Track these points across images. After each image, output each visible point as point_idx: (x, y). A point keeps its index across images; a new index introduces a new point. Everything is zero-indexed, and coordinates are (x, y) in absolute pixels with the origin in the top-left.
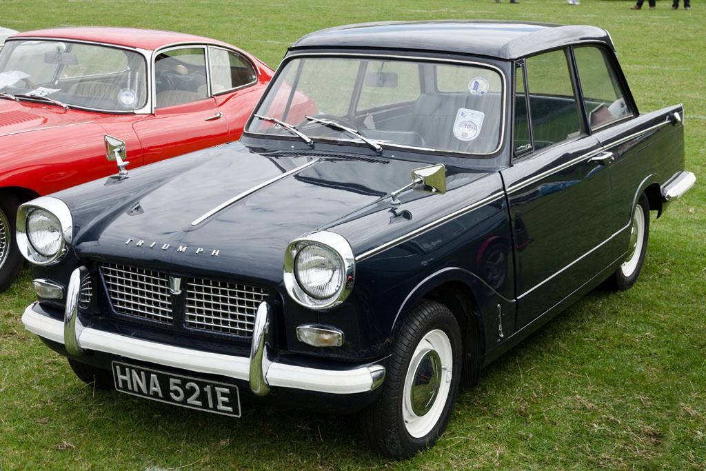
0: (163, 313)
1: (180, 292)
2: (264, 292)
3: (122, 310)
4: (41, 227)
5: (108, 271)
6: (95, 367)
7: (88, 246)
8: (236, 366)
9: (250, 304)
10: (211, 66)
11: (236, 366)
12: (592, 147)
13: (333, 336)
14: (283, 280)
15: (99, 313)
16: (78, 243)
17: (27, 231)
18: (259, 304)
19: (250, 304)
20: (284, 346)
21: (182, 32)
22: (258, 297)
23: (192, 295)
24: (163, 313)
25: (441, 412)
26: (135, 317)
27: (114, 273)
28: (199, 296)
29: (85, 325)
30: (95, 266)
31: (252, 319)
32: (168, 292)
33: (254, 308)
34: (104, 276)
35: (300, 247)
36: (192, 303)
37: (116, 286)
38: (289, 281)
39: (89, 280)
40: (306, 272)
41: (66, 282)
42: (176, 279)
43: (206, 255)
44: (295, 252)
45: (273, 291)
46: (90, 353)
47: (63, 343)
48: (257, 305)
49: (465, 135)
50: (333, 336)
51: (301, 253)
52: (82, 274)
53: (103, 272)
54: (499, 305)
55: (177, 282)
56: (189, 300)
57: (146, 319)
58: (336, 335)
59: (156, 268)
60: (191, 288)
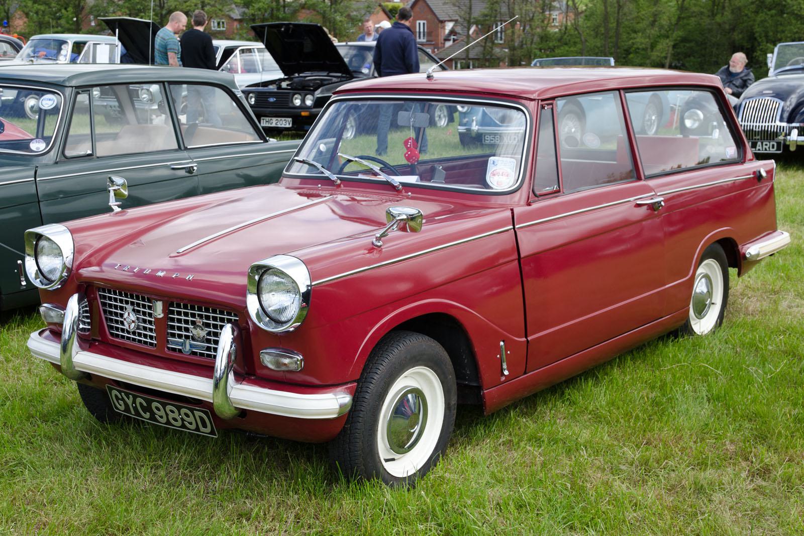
0: (151, 337)
1: (162, 316)
2: (235, 315)
3: (117, 336)
4: (277, 288)
5: (105, 297)
6: (94, 388)
7: (86, 272)
8: (195, 385)
9: (215, 326)
10: (360, 103)
11: (195, 385)
12: (148, 161)
13: (293, 361)
14: (246, 307)
15: (98, 338)
16: (80, 266)
17: (259, 294)
18: (223, 326)
19: (215, 326)
20: (247, 367)
21: (520, 65)
22: (222, 320)
23: (172, 320)
24: (151, 337)
25: (433, 448)
26: (145, 346)
27: (110, 299)
28: (179, 321)
29: (83, 348)
30: (88, 290)
31: (216, 342)
32: (150, 315)
33: (219, 331)
34: (101, 302)
35: (264, 270)
36: (173, 327)
37: (117, 313)
38: (252, 304)
39: (86, 306)
40: (267, 295)
41: (64, 306)
42: (158, 302)
43: (152, 277)
44: (257, 278)
45: (237, 313)
46: (244, 413)
47: (212, 402)
48: (221, 327)
49: (38, 148)
50: (293, 361)
51: (265, 277)
52: (80, 301)
53: (101, 299)
54: (502, 343)
55: (159, 306)
56: (170, 325)
57: (136, 344)
58: (296, 359)
59: (140, 292)
60: (172, 312)
